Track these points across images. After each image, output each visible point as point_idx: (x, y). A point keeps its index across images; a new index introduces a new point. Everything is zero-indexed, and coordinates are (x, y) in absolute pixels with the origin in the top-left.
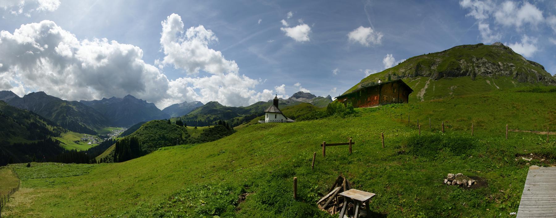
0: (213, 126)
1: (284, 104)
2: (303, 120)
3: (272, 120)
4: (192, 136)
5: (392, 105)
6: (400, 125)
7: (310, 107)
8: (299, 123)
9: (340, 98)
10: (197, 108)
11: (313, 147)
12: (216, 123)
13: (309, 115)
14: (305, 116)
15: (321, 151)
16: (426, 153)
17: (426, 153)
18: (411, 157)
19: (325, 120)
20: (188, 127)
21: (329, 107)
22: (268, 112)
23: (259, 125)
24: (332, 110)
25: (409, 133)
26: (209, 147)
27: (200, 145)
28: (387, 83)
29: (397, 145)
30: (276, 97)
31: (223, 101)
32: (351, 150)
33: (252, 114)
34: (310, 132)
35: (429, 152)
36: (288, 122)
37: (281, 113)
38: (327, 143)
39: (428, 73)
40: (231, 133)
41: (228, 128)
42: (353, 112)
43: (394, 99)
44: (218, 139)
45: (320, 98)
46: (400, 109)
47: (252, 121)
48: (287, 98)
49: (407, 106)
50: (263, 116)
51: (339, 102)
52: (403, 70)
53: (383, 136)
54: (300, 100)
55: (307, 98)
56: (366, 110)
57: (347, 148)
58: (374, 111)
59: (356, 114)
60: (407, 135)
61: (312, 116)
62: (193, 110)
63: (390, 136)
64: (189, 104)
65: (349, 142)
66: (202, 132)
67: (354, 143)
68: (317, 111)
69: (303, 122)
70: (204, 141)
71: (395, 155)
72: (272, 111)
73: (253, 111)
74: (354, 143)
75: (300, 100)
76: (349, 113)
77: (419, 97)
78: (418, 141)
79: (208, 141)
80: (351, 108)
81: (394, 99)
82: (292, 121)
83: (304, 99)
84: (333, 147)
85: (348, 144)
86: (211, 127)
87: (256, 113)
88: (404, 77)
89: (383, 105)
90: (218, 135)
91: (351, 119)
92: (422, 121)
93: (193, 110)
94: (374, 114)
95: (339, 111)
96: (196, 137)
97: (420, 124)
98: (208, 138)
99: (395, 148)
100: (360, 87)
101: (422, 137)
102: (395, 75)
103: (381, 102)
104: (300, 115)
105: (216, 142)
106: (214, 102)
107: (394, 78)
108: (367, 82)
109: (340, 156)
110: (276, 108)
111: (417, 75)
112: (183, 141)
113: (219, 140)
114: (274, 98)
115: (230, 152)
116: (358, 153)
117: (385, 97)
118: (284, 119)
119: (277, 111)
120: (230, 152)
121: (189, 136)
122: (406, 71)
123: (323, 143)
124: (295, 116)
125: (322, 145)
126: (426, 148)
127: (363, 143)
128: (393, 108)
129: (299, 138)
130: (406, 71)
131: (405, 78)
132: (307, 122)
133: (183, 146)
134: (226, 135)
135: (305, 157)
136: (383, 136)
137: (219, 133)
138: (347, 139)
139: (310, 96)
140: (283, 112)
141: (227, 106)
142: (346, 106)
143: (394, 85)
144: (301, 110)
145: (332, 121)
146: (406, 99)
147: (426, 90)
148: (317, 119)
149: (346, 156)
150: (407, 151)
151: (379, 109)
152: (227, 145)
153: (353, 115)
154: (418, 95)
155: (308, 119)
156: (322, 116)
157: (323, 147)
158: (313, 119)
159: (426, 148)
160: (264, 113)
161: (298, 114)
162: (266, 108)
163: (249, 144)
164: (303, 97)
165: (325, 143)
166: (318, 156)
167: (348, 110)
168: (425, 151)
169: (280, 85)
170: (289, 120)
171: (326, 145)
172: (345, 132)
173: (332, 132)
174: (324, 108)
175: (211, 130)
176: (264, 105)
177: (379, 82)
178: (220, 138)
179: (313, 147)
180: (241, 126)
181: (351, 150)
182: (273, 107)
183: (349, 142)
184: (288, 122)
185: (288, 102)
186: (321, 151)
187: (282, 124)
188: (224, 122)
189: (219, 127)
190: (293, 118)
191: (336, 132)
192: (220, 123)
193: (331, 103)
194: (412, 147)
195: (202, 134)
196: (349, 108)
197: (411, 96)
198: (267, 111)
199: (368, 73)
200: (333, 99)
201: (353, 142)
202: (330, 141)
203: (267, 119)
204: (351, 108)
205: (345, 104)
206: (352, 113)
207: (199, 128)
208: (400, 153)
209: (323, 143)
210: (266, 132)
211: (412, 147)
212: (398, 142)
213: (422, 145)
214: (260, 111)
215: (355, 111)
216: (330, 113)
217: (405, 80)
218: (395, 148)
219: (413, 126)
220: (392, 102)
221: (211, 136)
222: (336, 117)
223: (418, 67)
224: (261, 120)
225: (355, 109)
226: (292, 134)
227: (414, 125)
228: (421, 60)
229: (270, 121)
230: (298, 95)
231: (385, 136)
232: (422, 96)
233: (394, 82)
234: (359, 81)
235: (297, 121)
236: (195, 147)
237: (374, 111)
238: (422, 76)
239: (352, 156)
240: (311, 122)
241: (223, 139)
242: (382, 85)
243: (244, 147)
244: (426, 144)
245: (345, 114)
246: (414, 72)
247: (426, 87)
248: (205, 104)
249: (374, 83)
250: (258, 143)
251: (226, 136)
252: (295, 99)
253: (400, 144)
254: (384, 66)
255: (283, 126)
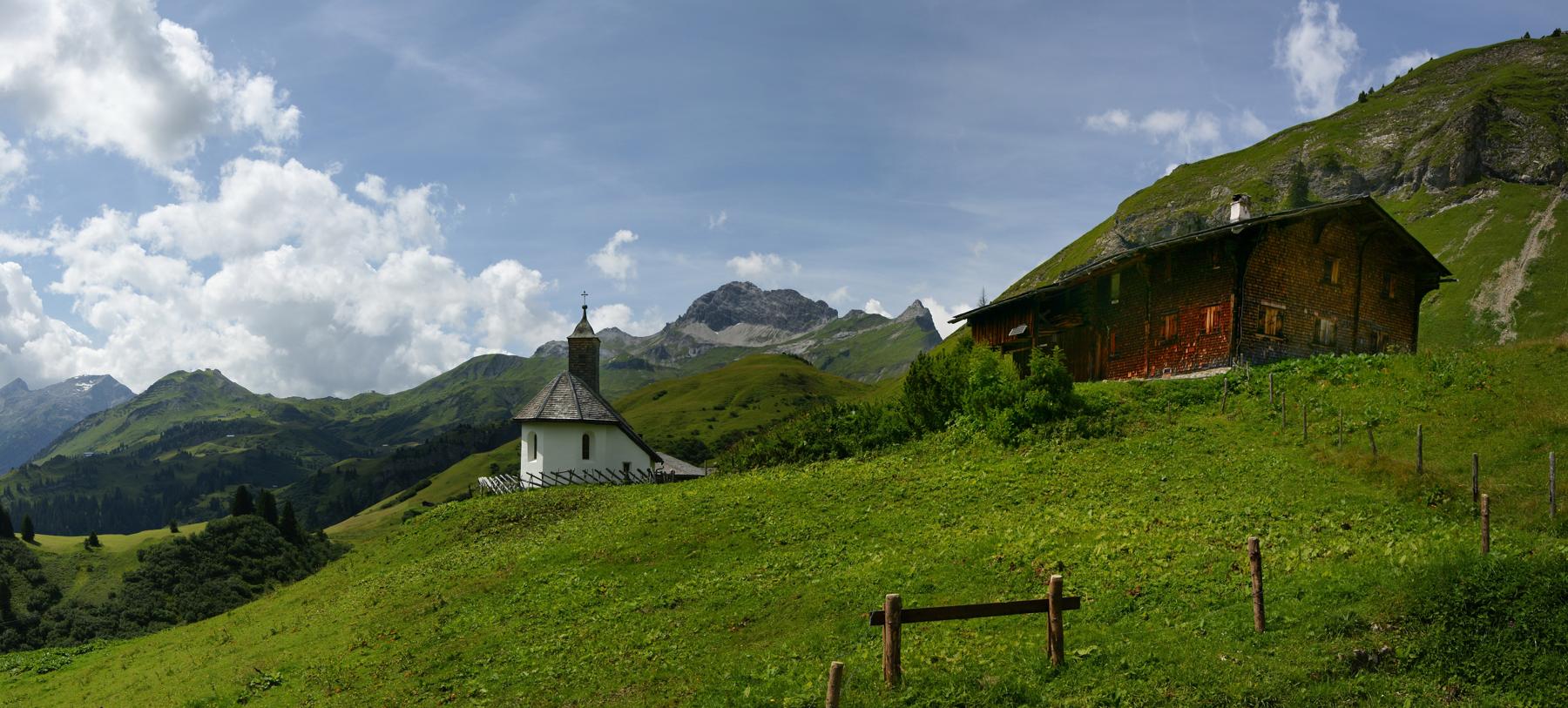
0: (199, 528)
1: (638, 364)
2: (760, 461)
3: (563, 467)
4: (70, 594)
5: (1319, 360)
6: (1363, 491)
7: (797, 383)
8: (733, 480)
9: (984, 321)
10: (94, 419)
11: (826, 629)
12: (215, 505)
13: (796, 432)
14: (772, 438)
15: (871, 654)
16: (1521, 664)
17: (1521, 664)
18: (1430, 687)
19: (893, 461)
20: (49, 543)
21: (920, 380)
22: (539, 422)
23: (480, 504)
24: (933, 396)
25: (1416, 543)
26: (179, 655)
27: (124, 647)
28: (1284, 223)
29: (1343, 612)
30: (584, 326)
31: (247, 361)
32: (1057, 641)
33: (468, 422)
34: (804, 537)
35: (1541, 662)
36: (661, 479)
37: (621, 425)
38: (907, 604)
39: (1546, 158)
40: (313, 565)
41: (289, 530)
42: (1071, 406)
43: (1326, 324)
44: (235, 603)
45: (859, 319)
46: (1371, 389)
47: (439, 481)
48: (647, 327)
49: (1409, 373)
50: (502, 450)
51: (982, 348)
52: (1387, 141)
53: (1256, 557)
54: (736, 336)
55: (782, 324)
56: (1150, 392)
57: (1031, 635)
58: (1200, 397)
59: (1093, 424)
60: (1409, 549)
61: (812, 438)
62: (68, 435)
63: (1298, 558)
64: (42, 396)
65: (1045, 593)
66: (134, 567)
67: (1074, 603)
68: (841, 401)
69: (755, 477)
70: (147, 621)
71: (1329, 675)
72: (562, 411)
73: (447, 418)
74: (1074, 603)
75: (736, 336)
76: (1043, 415)
77: (1489, 315)
78: (1472, 590)
79: (172, 622)
80: (1057, 385)
81: (1326, 324)
82: (686, 468)
83: (760, 329)
84: (946, 628)
85: (1041, 606)
86: (189, 530)
87: (463, 429)
88: (1392, 181)
89: (1260, 362)
90: (234, 579)
91: (1064, 456)
92: (1502, 465)
93: (68, 435)
94: (1200, 418)
95: (979, 405)
96: (99, 598)
97: (1492, 484)
98: (171, 601)
99: (1332, 629)
100: (1110, 246)
101: (1503, 567)
102: (1333, 167)
103: (1248, 344)
104: (737, 435)
105: (220, 621)
106: (198, 375)
107: (1328, 192)
108: (1158, 218)
109: (990, 680)
110: (584, 393)
111: (1475, 173)
112: (22, 627)
113: (240, 611)
114: (570, 331)
115: (312, 682)
116: (1100, 661)
117: (1272, 313)
118: (640, 461)
119: (595, 410)
120: (312, 682)
121: (56, 595)
122: (1405, 147)
123: (884, 606)
124: (709, 438)
125: (878, 619)
126: (1521, 636)
127: (1131, 602)
128: (1322, 385)
129: (738, 574)
130: (1405, 147)
131: (1400, 193)
132: (780, 474)
133: (21, 658)
134: (286, 575)
135: (779, 690)
136: (1256, 557)
137: (235, 566)
138: (1035, 577)
139: (797, 310)
140: (628, 417)
141: (283, 389)
142: (1025, 372)
143: (1331, 235)
144: (757, 401)
145: (954, 463)
146: (1407, 328)
147: (1533, 269)
148: (843, 454)
149: (1031, 683)
150: (1407, 649)
151: (1232, 387)
152: (287, 639)
153: (1068, 425)
154: (1479, 304)
155: (786, 454)
156: (877, 438)
157: (885, 632)
158: (822, 455)
159: (1521, 636)
160: (512, 431)
161: (725, 426)
162: (523, 394)
163: (428, 625)
164: (755, 319)
165: (896, 603)
166: (858, 683)
167: (1035, 396)
168: (1519, 656)
169: (599, 239)
170: (672, 465)
171: (904, 615)
172: (1019, 536)
173: (943, 538)
174: (888, 391)
175: (186, 553)
176: (509, 377)
177: (1236, 212)
178: (246, 596)
179: (826, 629)
180: (372, 516)
181: (1057, 641)
182: (566, 389)
183: (1045, 593)
184: (661, 479)
185: (662, 353)
186: (871, 654)
187: (631, 492)
188: (268, 499)
189: (234, 529)
190: (693, 452)
191: (963, 537)
192: (242, 504)
193: (933, 352)
194: (1437, 629)
195: (131, 579)
196: (1040, 383)
197: (1433, 307)
198: (530, 413)
199: (1187, 132)
200: (945, 329)
201: (1067, 593)
202: (929, 588)
203: (532, 467)
204: (1057, 385)
205: (1021, 360)
206: (1062, 415)
207: (110, 541)
208: (1359, 662)
209: (884, 606)
210: (528, 547)
211: (1437, 629)
212: (1348, 596)
213: (1498, 619)
214: (482, 416)
215: (1078, 403)
216: (925, 412)
217: (1397, 203)
218: (1332, 629)
219: (1434, 496)
220: (1316, 345)
221: (180, 590)
222: (963, 442)
223: (1485, 121)
224: (494, 471)
225: (1080, 389)
226: (693, 552)
227: (1451, 492)
228: (1501, 76)
229: (552, 478)
230: (723, 306)
231: (1271, 557)
232: (1503, 306)
233: (1323, 219)
234: (1104, 209)
235: (722, 472)
236: (95, 658)
237: (1200, 397)
238: (1508, 176)
239: (1064, 682)
240: (806, 473)
241: (263, 603)
242: (1253, 232)
243: (399, 647)
244: (1522, 612)
245: (1020, 423)
246: (1459, 150)
247: (1532, 250)
248: (138, 389)
249: (1199, 223)
250: (484, 617)
251: (285, 580)
252: (701, 331)
253: (1362, 609)
254: (1282, 80)
255: (640, 503)
